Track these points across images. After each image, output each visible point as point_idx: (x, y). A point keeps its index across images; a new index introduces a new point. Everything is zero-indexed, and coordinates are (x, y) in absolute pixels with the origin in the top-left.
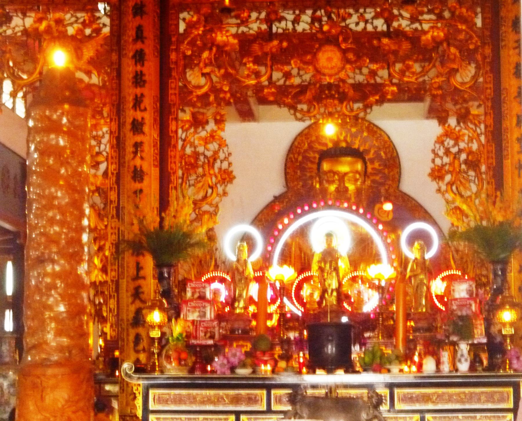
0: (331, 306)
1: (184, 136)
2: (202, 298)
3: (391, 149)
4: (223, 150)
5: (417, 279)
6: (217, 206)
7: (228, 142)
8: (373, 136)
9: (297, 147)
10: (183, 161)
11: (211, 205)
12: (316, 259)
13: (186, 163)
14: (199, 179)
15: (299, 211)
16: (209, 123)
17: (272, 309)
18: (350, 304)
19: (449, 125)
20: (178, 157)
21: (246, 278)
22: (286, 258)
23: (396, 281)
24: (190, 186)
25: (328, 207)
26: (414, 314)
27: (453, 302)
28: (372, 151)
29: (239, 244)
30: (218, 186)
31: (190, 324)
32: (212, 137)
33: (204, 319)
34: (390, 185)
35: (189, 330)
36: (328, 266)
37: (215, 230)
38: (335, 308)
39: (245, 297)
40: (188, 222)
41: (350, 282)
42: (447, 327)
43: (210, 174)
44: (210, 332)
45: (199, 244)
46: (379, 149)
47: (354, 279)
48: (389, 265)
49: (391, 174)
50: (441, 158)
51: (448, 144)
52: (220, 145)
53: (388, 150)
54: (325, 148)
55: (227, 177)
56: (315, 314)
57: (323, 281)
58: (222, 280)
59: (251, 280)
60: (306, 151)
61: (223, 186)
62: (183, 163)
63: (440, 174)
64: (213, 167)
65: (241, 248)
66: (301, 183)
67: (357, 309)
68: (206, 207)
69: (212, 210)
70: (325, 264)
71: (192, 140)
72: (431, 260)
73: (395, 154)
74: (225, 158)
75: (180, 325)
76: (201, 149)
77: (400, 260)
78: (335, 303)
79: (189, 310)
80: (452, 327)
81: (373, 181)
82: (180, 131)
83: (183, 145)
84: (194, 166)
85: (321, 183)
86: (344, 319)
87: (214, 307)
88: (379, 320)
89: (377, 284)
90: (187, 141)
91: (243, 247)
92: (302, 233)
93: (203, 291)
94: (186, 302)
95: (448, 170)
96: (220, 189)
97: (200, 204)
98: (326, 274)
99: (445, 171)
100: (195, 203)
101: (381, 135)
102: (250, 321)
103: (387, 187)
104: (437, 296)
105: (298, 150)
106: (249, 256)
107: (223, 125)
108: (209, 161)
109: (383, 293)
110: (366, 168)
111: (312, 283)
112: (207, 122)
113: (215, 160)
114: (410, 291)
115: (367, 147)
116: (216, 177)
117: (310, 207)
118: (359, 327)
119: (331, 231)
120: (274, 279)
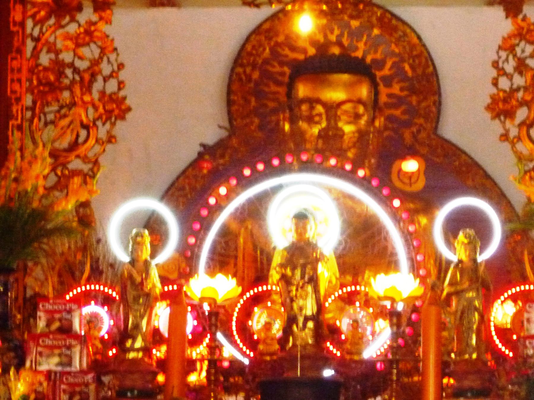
0: (305, 346)
1: (36, 33)
2: (66, 330)
3: (424, 61)
4: (108, 59)
5: (462, 300)
6: (96, 163)
7: (116, 44)
8: (391, 35)
9: (250, 54)
10: (34, 77)
11: (85, 159)
12: (277, 260)
13: (40, 82)
14: (63, 111)
15: (247, 172)
16: (84, 8)
17: (200, 351)
18: (339, 344)
19: (524, 19)
20: (24, 72)
21: (148, 295)
22: (223, 260)
23: (423, 302)
24: (46, 124)
25: (306, 167)
26: (455, 362)
27: (527, 342)
28: (389, 64)
29: (134, 231)
30: (99, 123)
31: (41, 378)
32: (89, 34)
33: (68, 369)
34: (421, 125)
35: (40, 389)
36: (298, 273)
37: (93, 205)
38: (310, 351)
39: (144, 329)
40: (41, 191)
41: (340, 304)
42: (516, 388)
43: (84, 102)
44: (80, 393)
45: (63, 230)
46: (402, 60)
47: (349, 299)
48: (411, 275)
49: (424, 104)
50: (510, 77)
51: (523, 51)
52: (103, 50)
53: (417, 61)
54: (301, 57)
55: (116, 108)
56: (275, 361)
57: (288, 300)
58: (107, 301)
59: (156, 300)
60: (266, 62)
61: (108, 125)
62: (35, 82)
63: (508, 107)
64: (89, 90)
65: (139, 239)
66: (256, 121)
67: (350, 353)
68: (75, 164)
69: (86, 168)
70: (293, 269)
71: (51, 39)
72: (488, 263)
73: (431, 69)
74: (113, 71)
75: (25, 380)
76: (67, 57)
77: (438, 264)
78: (310, 341)
79: (41, 354)
80: (524, 387)
81: (389, 119)
82: (29, 23)
83: (35, 48)
84: (54, 88)
85: (293, 121)
86: (328, 373)
87: (88, 349)
88: (391, 373)
89: (389, 307)
90: (43, 41)
91: (142, 236)
92: (254, 211)
93: (68, 317)
94: (36, 338)
95: (522, 98)
96: (102, 131)
97: (66, 157)
98: (294, 288)
99: (517, 100)
100: (54, 154)
101: (405, 34)
102: (155, 374)
103: (414, 129)
104: (497, 328)
105: (252, 59)
106: (153, 255)
107: (108, 12)
108: (82, 78)
109: (399, 325)
110: (377, 94)
111: (269, 304)
112: (80, 8)
113: (93, 76)
114: (449, 320)
115: (379, 56)
116: (96, 108)
117: (268, 163)
118: (355, 387)
119: (306, 210)
120: (199, 296)
